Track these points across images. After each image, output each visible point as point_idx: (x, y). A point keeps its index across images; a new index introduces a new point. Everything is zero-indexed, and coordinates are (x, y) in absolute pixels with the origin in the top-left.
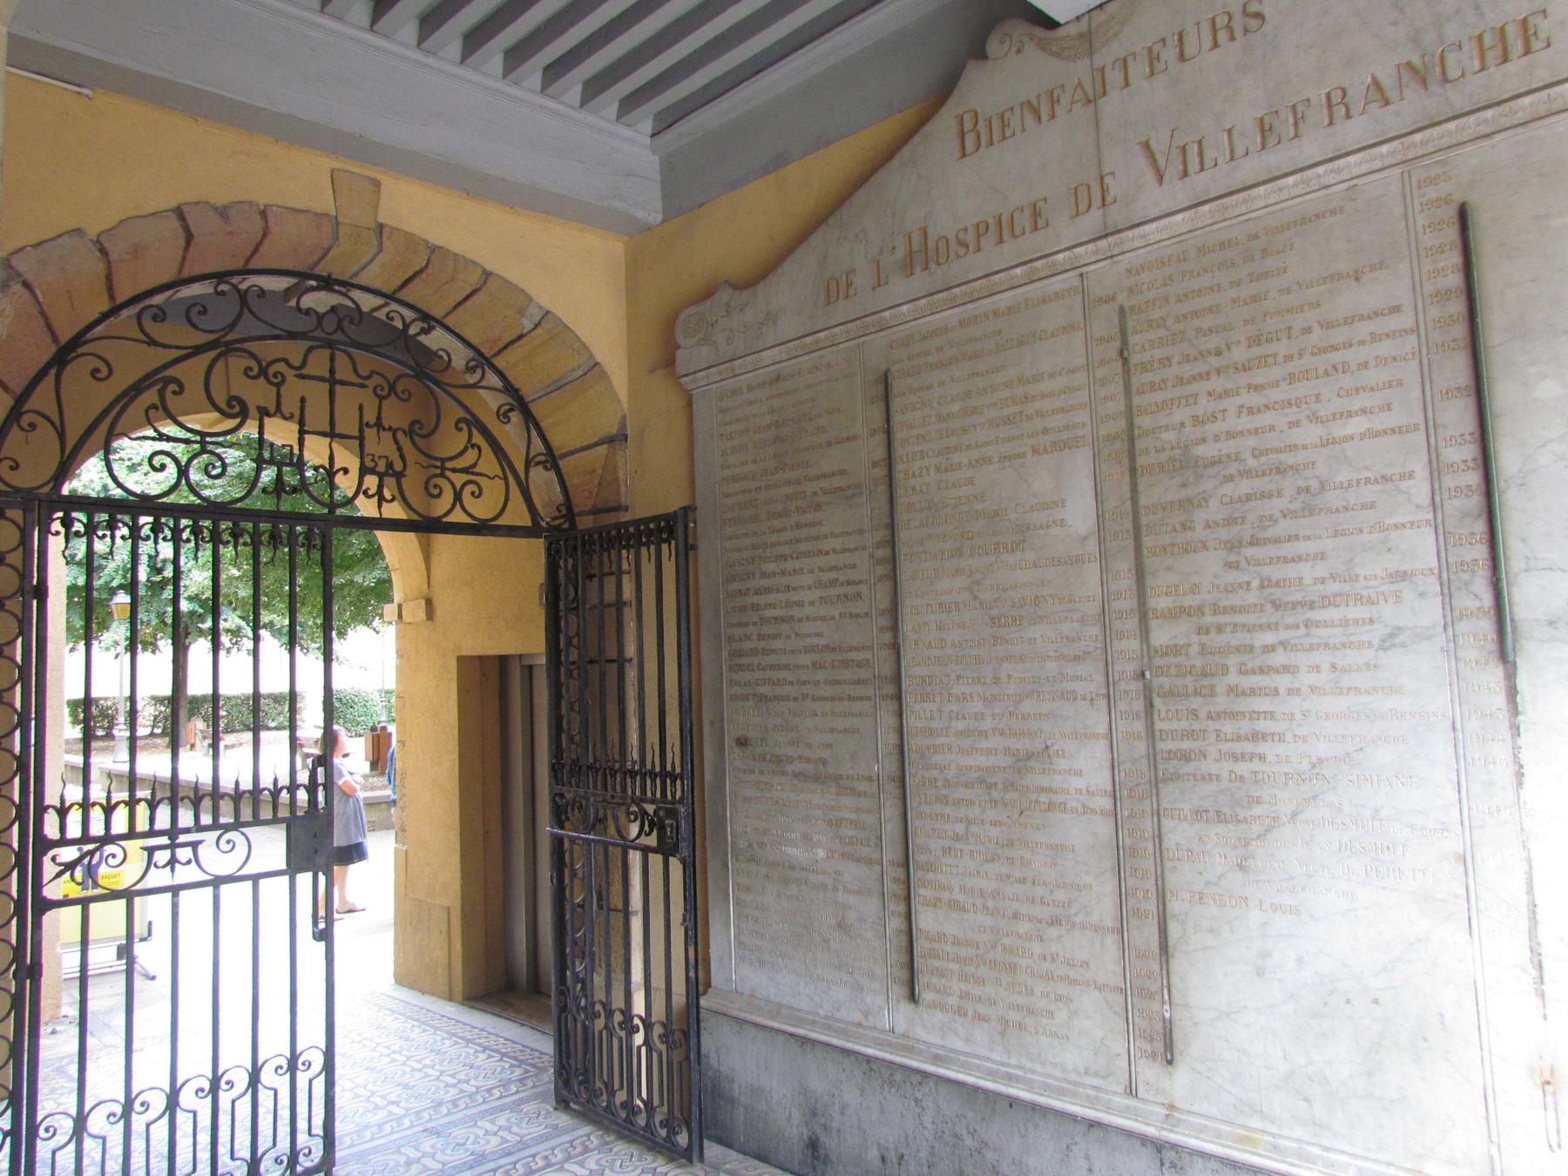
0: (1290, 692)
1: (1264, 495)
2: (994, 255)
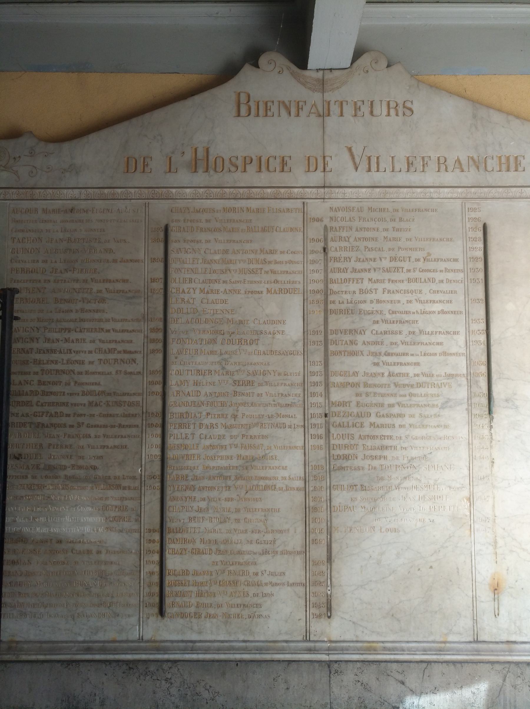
0: (401, 426)
1: (393, 333)
2: (251, 177)
